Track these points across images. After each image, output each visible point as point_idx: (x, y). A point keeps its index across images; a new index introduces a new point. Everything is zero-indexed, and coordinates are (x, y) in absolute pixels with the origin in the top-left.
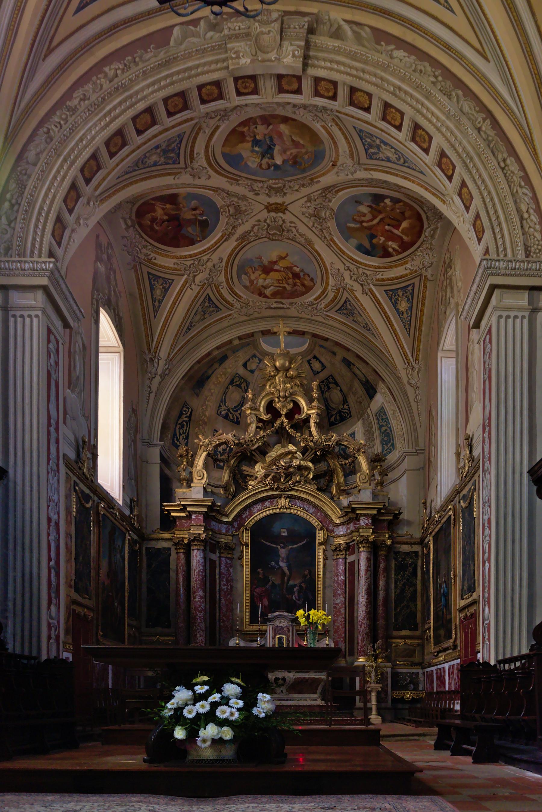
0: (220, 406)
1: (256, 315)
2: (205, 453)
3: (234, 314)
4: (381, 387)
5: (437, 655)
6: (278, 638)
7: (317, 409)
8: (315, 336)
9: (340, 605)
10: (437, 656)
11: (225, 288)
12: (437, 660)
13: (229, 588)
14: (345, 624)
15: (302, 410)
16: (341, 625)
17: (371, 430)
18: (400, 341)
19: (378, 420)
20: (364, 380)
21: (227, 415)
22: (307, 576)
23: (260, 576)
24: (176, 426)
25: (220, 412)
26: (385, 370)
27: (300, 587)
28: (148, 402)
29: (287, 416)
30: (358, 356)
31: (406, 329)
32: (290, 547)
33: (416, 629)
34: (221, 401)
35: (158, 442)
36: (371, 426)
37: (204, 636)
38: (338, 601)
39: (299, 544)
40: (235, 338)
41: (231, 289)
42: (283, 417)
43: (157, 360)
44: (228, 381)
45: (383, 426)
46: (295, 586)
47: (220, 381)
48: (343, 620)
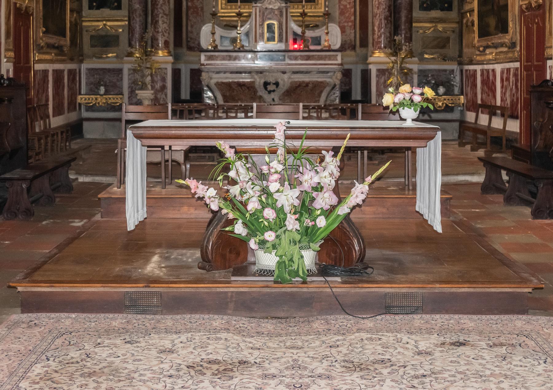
5: (484, 51)
6: (268, 25)
10: (483, 53)
12: (483, 58)
33: (450, 8)
37: (168, 22)
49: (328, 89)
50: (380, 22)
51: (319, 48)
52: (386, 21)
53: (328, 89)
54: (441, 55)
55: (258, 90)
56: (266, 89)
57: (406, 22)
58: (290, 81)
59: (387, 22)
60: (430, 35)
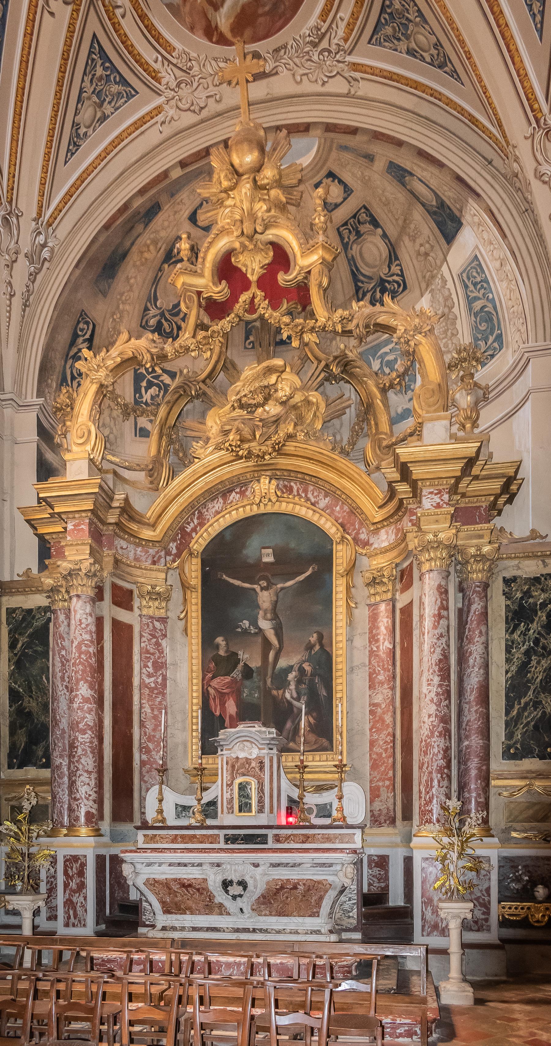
0: (146, 309)
1: (213, 107)
2: (94, 388)
3: (166, 107)
4: (473, 211)
7: (324, 247)
8: (330, 128)
9: (383, 706)
11: (128, 14)
13: (160, 680)
14: (394, 748)
15: (292, 264)
16: (386, 750)
17: (450, 311)
18: (517, 59)
19: (466, 287)
20: (434, 203)
21: (159, 324)
22: (314, 646)
23: (222, 653)
24: (66, 362)
25: (147, 322)
26: (483, 172)
27: (302, 671)
28: (9, 318)
29: (261, 283)
30: (422, 154)
31: (534, 16)
32: (280, 586)
34: (149, 300)
35: (35, 399)
36: (449, 303)
38: (379, 699)
39: (301, 578)
40: (173, 167)
41: (143, 17)
42: (254, 289)
43: (14, 220)
44: (161, 254)
45: (476, 299)
46: (290, 669)
47: (146, 259)
48: (389, 739)
49: (331, 895)
50: (429, 776)
51: (327, 821)
52: (439, 775)
53: (331, 895)
54: (540, 832)
55: (215, 893)
56: (227, 892)
57: (478, 777)
58: (266, 879)
59: (442, 777)
60: (521, 800)
